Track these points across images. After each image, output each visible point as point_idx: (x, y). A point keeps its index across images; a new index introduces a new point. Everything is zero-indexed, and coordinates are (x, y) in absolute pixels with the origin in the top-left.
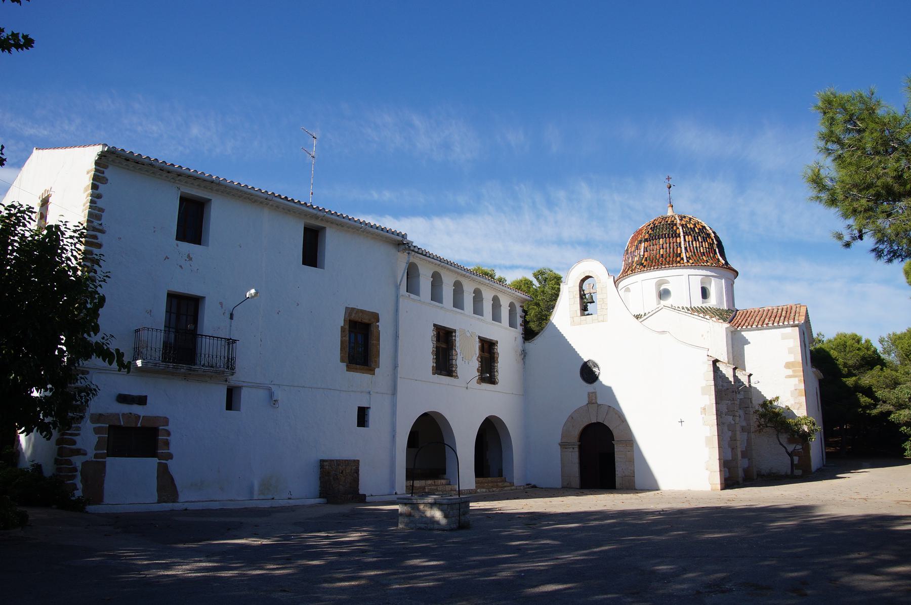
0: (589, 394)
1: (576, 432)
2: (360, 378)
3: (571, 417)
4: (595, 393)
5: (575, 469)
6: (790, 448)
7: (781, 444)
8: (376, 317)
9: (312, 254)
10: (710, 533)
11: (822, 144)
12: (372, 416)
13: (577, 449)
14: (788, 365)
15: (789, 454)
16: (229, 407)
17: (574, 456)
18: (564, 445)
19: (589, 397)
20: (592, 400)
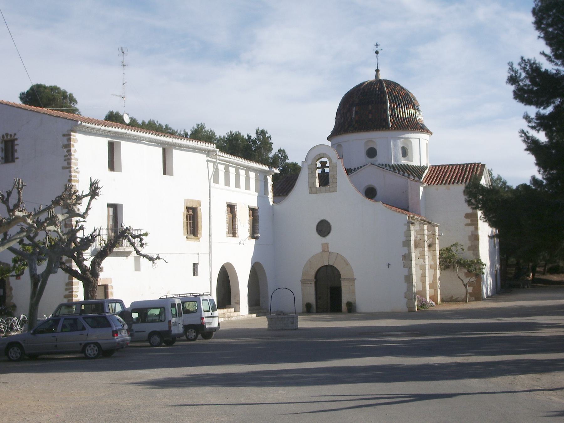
0: (322, 244)
1: (313, 273)
2: (193, 243)
3: (309, 261)
4: (327, 244)
5: (312, 299)
6: (466, 280)
7: (459, 277)
8: (199, 203)
9: (64, 135)
10: (446, 339)
11: (520, 134)
12: (200, 268)
13: (313, 285)
14: (231, 132)
15: (465, 285)
16: (194, 275)
17: (311, 289)
18: (304, 282)
19: (323, 247)
20: (325, 249)
